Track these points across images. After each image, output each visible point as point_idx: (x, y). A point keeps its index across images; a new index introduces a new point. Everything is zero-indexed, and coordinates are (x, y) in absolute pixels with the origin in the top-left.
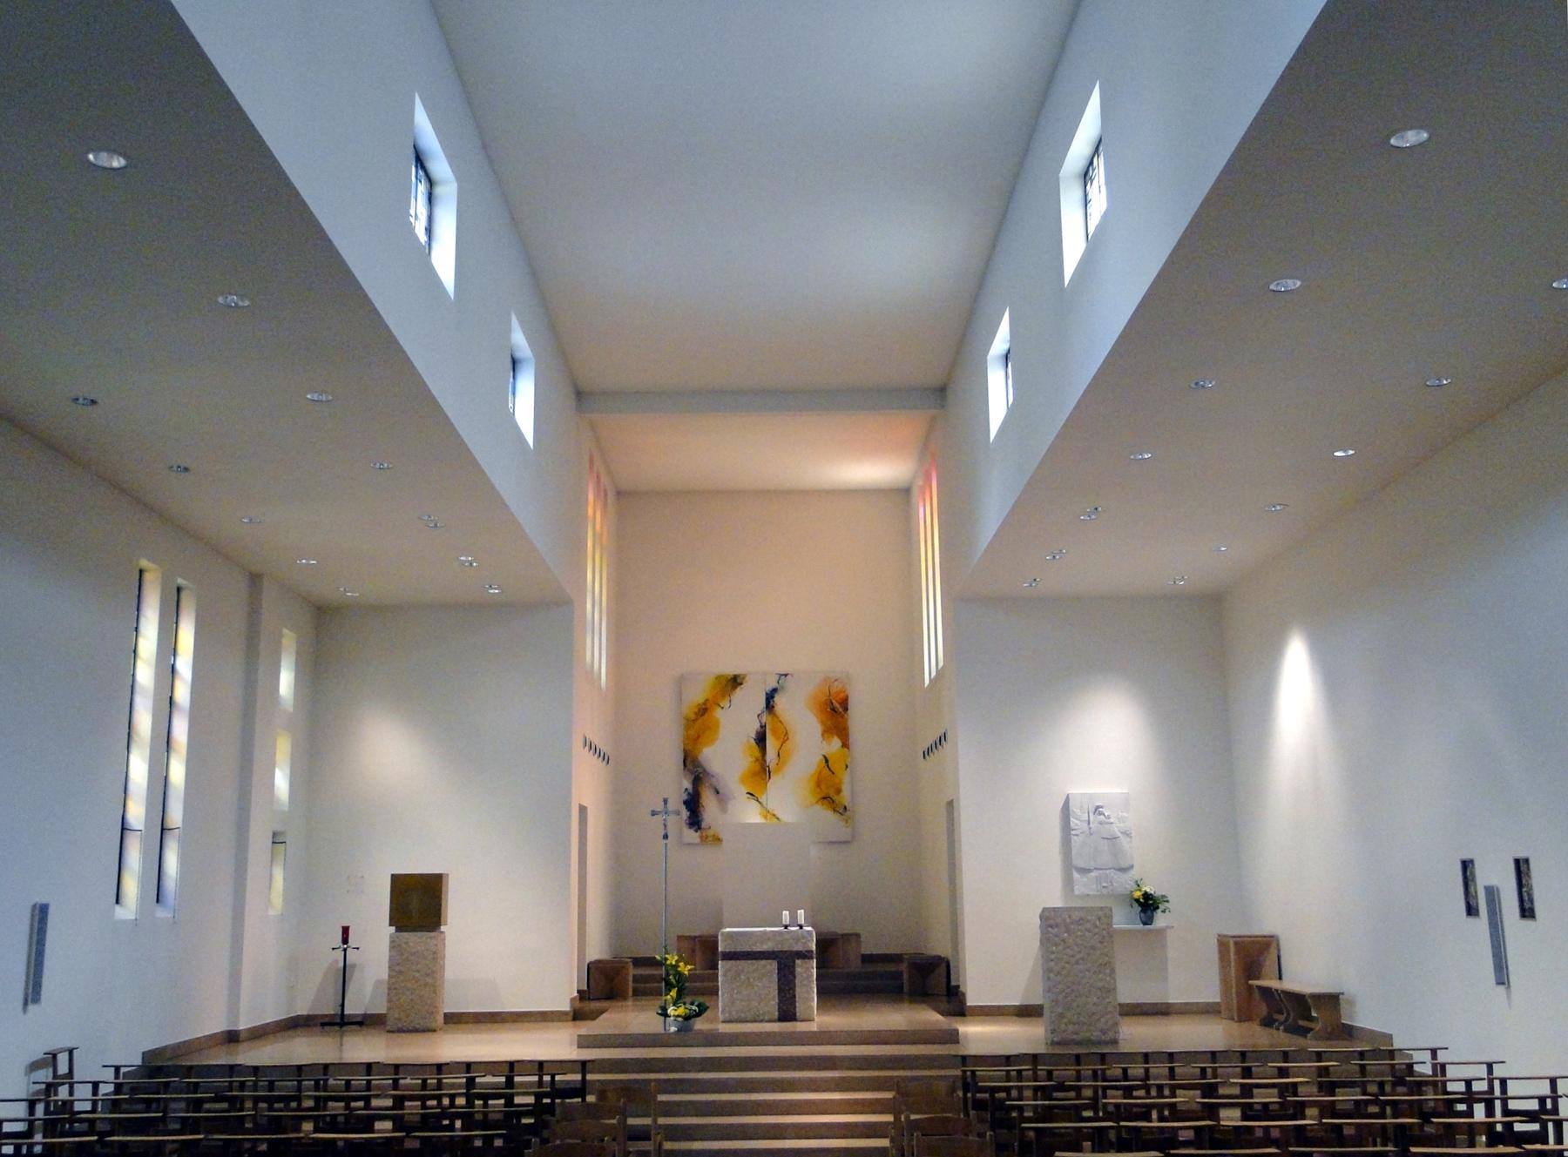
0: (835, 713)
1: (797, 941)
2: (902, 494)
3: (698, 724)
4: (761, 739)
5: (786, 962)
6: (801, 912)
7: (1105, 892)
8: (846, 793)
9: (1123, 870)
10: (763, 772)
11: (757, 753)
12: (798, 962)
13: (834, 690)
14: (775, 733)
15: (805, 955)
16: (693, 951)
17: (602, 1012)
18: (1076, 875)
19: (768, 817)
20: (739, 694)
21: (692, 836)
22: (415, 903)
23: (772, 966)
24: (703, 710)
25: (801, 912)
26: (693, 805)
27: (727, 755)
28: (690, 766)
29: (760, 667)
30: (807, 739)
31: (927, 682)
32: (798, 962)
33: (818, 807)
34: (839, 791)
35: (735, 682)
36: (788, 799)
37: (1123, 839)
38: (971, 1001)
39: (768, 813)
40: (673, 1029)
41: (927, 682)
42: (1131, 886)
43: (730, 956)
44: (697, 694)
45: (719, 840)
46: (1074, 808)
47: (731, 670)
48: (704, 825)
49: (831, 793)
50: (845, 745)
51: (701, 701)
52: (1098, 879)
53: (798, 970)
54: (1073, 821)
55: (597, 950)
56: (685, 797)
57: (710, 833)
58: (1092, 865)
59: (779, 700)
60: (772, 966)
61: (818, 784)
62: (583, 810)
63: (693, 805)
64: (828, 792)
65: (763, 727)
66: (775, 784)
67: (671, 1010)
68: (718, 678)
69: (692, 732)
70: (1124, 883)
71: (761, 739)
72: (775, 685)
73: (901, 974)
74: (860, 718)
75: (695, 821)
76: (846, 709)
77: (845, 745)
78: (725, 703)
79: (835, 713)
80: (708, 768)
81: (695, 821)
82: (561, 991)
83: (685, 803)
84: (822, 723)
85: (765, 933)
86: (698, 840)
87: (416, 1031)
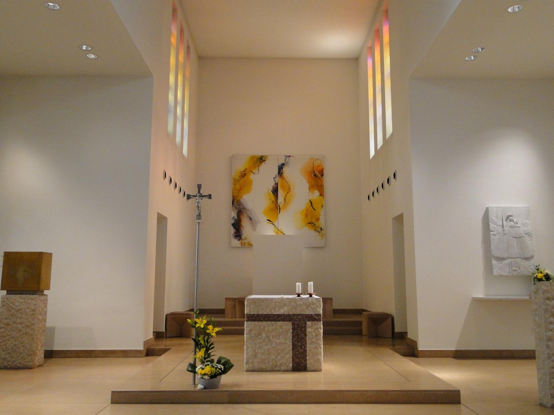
0: (316, 177)
1: (308, 306)
2: (354, 62)
3: (241, 182)
4: (275, 191)
5: (299, 323)
6: (311, 284)
7: (515, 273)
8: (322, 218)
9: (527, 259)
10: (276, 208)
11: (273, 199)
12: (309, 323)
13: (316, 165)
14: (283, 187)
15: (314, 318)
16: (235, 307)
17: (165, 351)
18: (494, 262)
19: (279, 232)
20: (263, 166)
21: (236, 243)
22: (20, 275)
23: (288, 326)
24: (244, 175)
25: (311, 284)
26: (237, 226)
27: (256, 199)
28: (236, 205)
29: (275, 153)
30: (300, 191)
31: (372, 153)
32: (309, 323)
33: (306, 228)
34: (318, 220)
35: (261, 159)
36: (290, 223)
37: (527, 239)
38: (421, 347)
39: (278, 231)
40: (200, 386)
41: (372, 153)
42: (532, 270)
43: (253, 318)
44: (241, 166)
45: (251, 245)
46: (492, 216)
47: (259, 153)
48: (242, 238)
49: (314, 220)
50: (322, 195)
51: (243, 169)
52: (510, 265)
53: (309, 330)
54: (492, 226)
55: (176, 304)
56: (233, 221)
57: (246, 241)
58: (505, 255)
59: (285, 170)
60: (288, 326)
61: (306, 216)
62: (162, 220)
63: (237, 226)
64: (312, 220)
65: (277, 184)
66: (282, 215)
67: (199, 367)
68: (253, 157)
69: (238, 187)
70: (528, 268)
71: (275, 191)
72: (283, 162)
73: (360, 323)
74: (330, 180)
75: (238, 235)
76: (322, 175)
77: (322, 195)
78: (255, 171)
79: (316, 177)
80: (246, 207)
81: (238, 235)
82: (138, 336)
83: (233, 225)
84: (309, 182)
85: (282, 299)
86: (240, 245)
87: (17, 368)
